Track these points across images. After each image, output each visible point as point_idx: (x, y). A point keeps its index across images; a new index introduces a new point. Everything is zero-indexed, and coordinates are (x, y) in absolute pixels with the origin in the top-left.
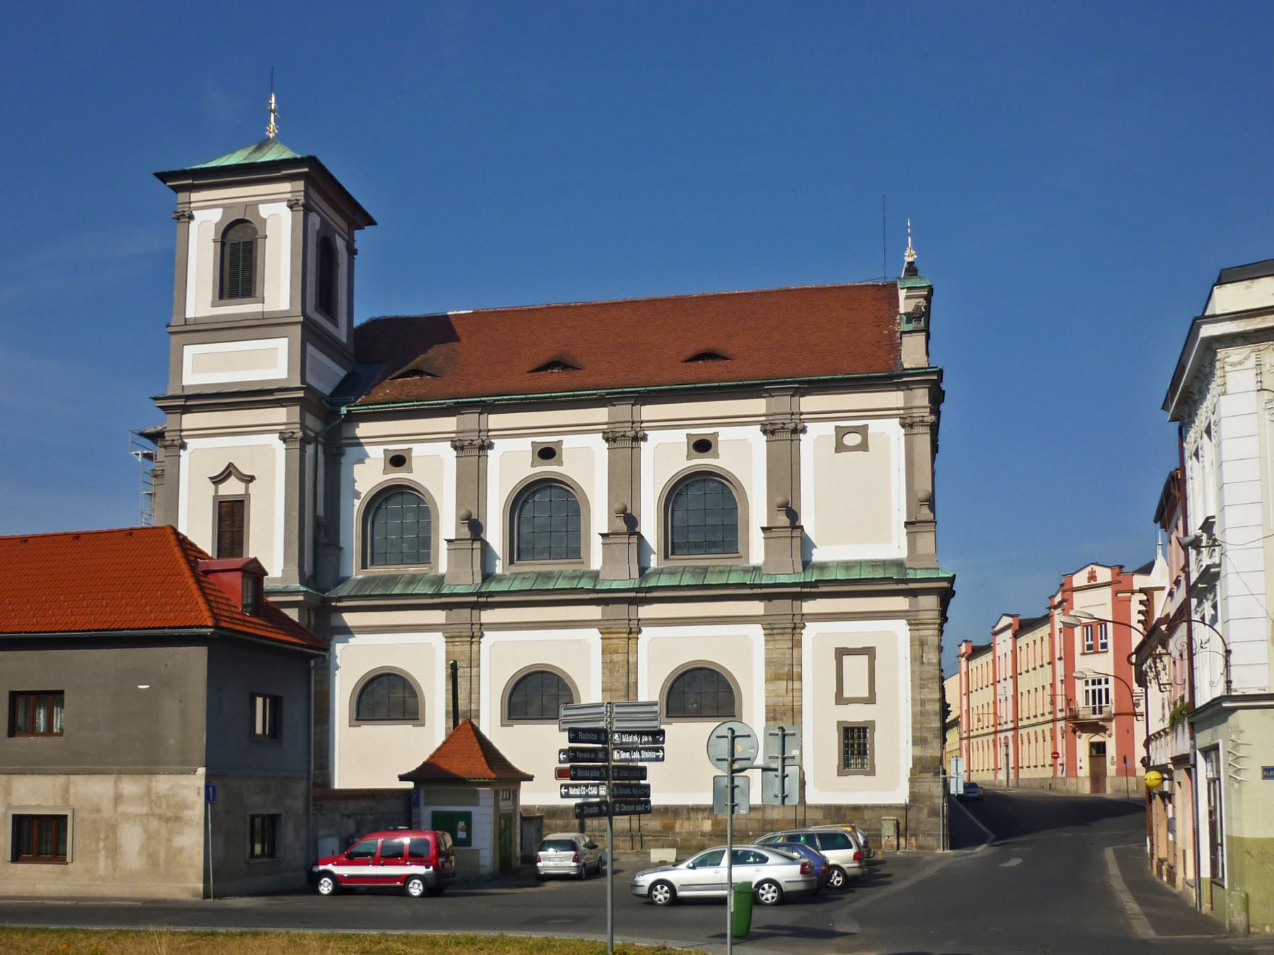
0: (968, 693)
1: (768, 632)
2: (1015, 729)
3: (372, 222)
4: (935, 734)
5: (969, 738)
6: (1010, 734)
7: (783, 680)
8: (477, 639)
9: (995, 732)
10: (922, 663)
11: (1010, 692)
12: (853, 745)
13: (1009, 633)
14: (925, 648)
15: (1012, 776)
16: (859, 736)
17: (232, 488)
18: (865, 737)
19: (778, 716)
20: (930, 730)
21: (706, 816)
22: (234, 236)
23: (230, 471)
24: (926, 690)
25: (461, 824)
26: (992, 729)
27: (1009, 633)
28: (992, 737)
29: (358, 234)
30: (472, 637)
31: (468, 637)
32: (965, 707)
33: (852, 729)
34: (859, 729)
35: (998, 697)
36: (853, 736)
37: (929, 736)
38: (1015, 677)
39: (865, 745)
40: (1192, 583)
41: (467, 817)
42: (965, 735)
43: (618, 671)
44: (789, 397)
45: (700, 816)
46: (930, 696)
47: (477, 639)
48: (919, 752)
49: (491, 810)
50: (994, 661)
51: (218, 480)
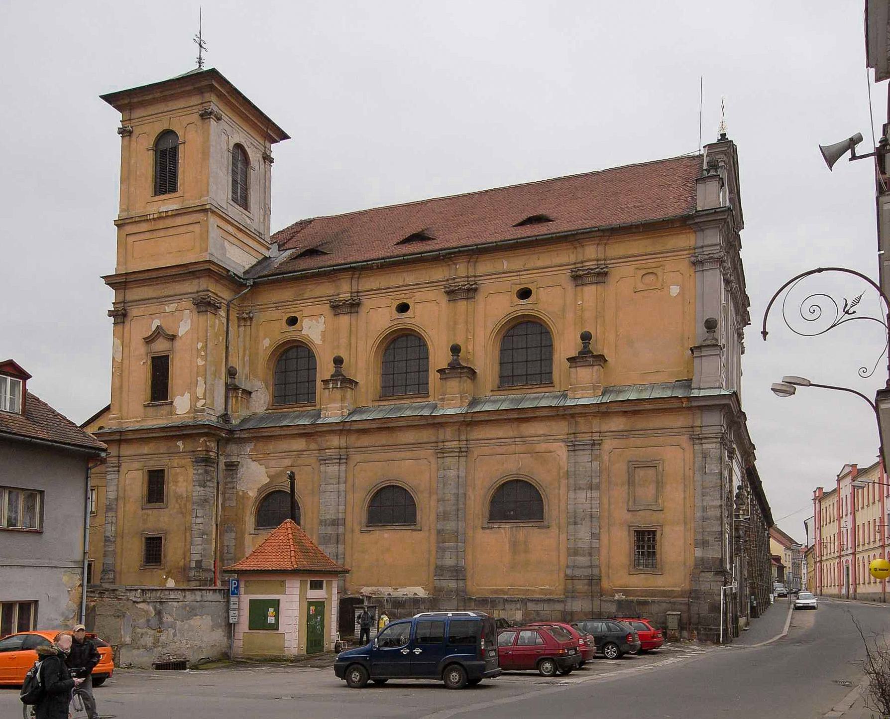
0: (820, 528)
1: (570, 448)
2: (854, 554)
3: (285, 137)
4: (716, 538)
5: (820, 561)
6: (850, 558)
7: (584, 489)
8: (344, 461)
9: (839, 557)
10: (705, 473)
11: (850, 525)
12: (643, 547)
13: (849, 479)
14: (708, 459)
15: (851, 592)
16: (649, 539)
17: (161, 346)
18: (654, 540)
19: (579, 520)
20: (712, 533)
21: (519, 608)
22: (163, 146)
23: (159, 333)
24: (708, 498)
25: (271, 610)
26: (837, 554)
27: (849, 479)
28: (837, 561)
29: (274, 147)
30: (340, 459)
31: (337, 459)
32: (818, 538)
33: (643, 532)
34: (649, 532)
35: (842, 530)
36: (643, 539)
37: (711, 539)
38: (854, 513)
39: (654, 547)
40: (878, 285)
41: (276, 604)
42: (818, 559)
43: (450, 484)
44: (595, 246)
45: (513, 606)
46: (711, 503)
47: (344, 461)
48: (699, 553)
49: (297, 598)
50: (838, 502)
51: (149, 340)
